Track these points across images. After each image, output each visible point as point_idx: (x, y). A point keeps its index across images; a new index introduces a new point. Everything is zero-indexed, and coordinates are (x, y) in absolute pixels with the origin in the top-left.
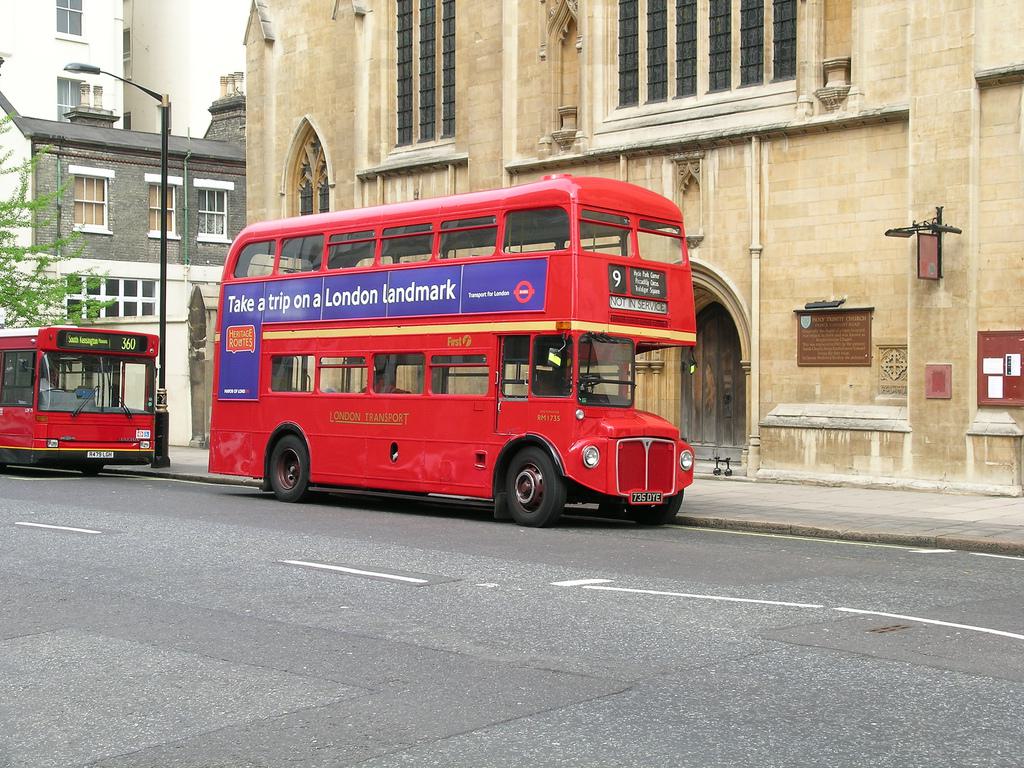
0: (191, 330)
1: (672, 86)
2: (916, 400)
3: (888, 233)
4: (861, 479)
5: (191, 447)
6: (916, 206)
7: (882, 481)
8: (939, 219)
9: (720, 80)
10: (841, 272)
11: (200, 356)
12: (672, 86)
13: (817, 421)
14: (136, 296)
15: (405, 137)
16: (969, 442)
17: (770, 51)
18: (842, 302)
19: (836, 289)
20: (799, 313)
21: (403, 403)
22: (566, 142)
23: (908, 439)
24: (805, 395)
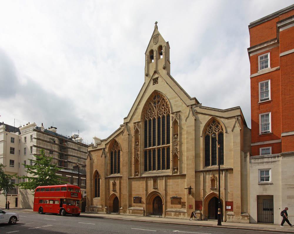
2: (187, 209)
4: (180, 218)
6: (187, 186)
7: (183, 218)
8: (190, 187)
9: (159, 169)
10: (176, 193)
13: (174, 211)
17: (152, 152)
19: (176, 195)
20: (171, 198)
21: (51, 204)
23: (186, 214)
24: (172, 208)
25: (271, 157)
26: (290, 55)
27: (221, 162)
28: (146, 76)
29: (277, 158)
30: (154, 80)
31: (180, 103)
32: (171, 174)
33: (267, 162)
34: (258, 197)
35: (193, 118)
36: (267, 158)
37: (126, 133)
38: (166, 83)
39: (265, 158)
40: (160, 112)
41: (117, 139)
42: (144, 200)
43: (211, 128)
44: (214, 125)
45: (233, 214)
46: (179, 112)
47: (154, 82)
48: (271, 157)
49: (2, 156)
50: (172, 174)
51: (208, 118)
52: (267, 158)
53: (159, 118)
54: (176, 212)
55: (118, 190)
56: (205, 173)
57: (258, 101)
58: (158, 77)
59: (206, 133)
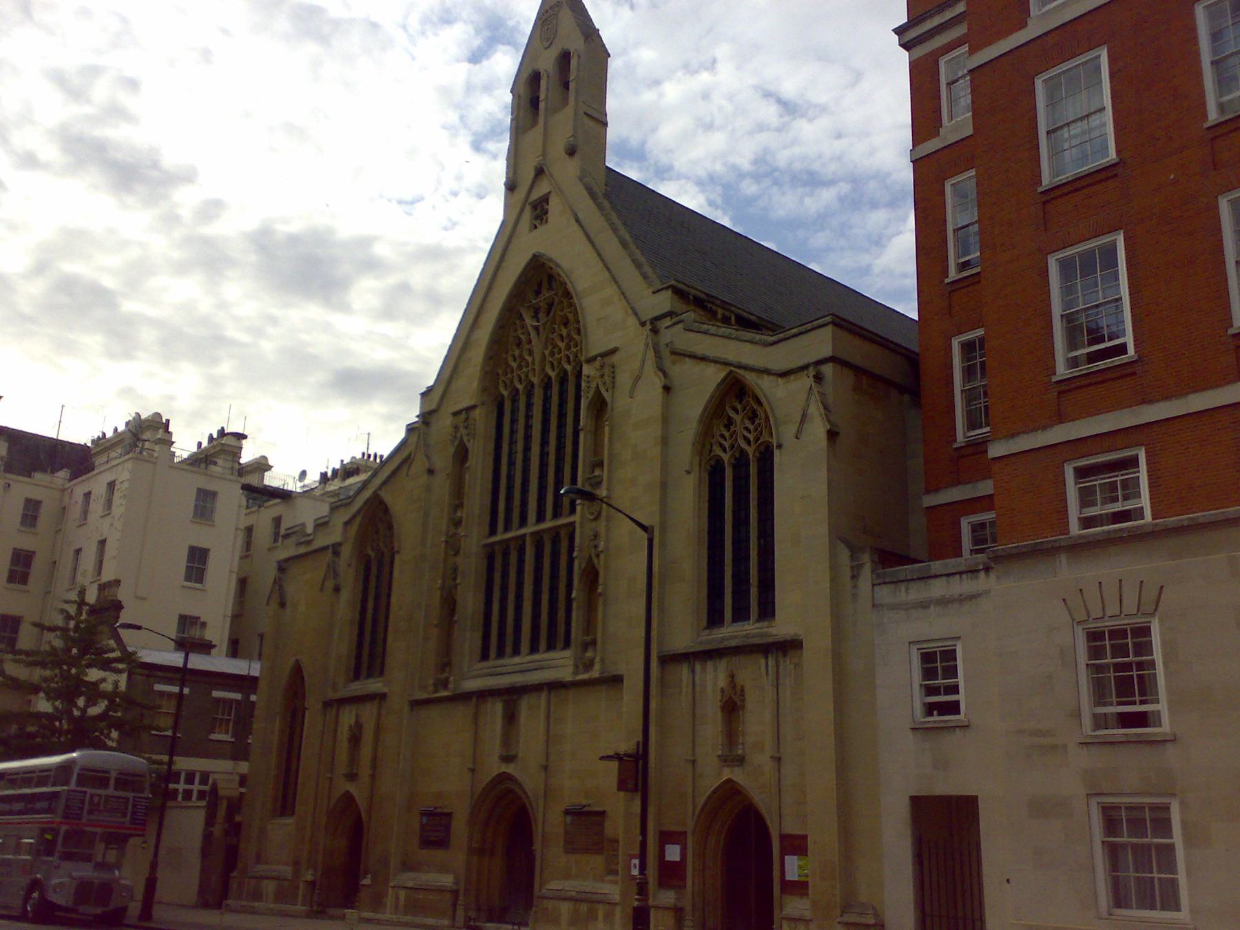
0: (206, 812)
1: (509, 649)
3: (602, 758)
5: (194, 907)
9: (534, 649)
11: (211, 833)
12: (509, 649)
14: (179, 783)
15: (357, 676)
16: (390, 889)
18: (589, 805)
22: (445, 684)
23: (618, 910)
25: (960, 573)
26: (994, 62)
27: (767, 611)
28: (508, 191)
29: (982, 575)
30: (535, 206)
31: (617, 311)
32: (566, 674)
33: (944, 602)
34: (918, 803)
35: (657, 382)
36: (941, 576)
37: (419, 466)
38: (573, 221)
39: (936, 576)
40: (552, 354)
41: (386, 496)
42: (460, 828)
43: (729, 423)
44: (739, 407)
45: (808, 914)
46: (613, 351)
47: (536, 218)
48: (960, 573)
49: (828, 319)
50: (575, 673)
51: (713, 376)
52: (944, 578)
53: (547, 385)
54: (576, 900)
55: (365, 772)
56: (698, 667)
57: (945, 273)
58: (550, 192)
59: (711, 451)
